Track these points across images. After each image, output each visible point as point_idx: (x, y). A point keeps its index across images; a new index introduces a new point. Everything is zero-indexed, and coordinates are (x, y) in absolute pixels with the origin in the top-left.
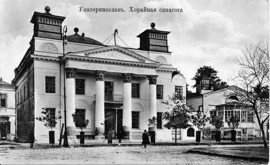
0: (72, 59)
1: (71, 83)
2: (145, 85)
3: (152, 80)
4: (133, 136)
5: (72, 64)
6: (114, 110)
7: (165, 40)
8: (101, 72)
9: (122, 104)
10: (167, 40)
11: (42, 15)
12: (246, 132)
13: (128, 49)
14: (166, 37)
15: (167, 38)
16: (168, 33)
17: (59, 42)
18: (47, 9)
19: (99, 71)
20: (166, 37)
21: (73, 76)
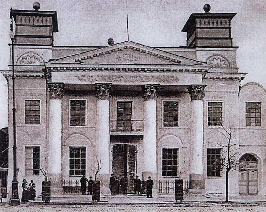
0: (56, 69)
1: (57, 107)
2: (183, 105)
3: (194, 92)
4: (160, 188)
5: (57, 78)
6: (124, 148)
7: (226, 28)
8: (200, 87)
9: (141, 137)
10: (230, 28)
11: (201, 16)
12: (210, 178)
13: (158, 49)
14: (228, 24)
15: (230, 25)
16: (230, 16)
17: (204, 50)
18: (207, 8)
19: (194, 85)
20: (228, 24)
21: (58, 95)
